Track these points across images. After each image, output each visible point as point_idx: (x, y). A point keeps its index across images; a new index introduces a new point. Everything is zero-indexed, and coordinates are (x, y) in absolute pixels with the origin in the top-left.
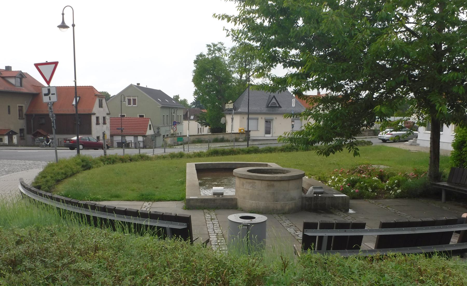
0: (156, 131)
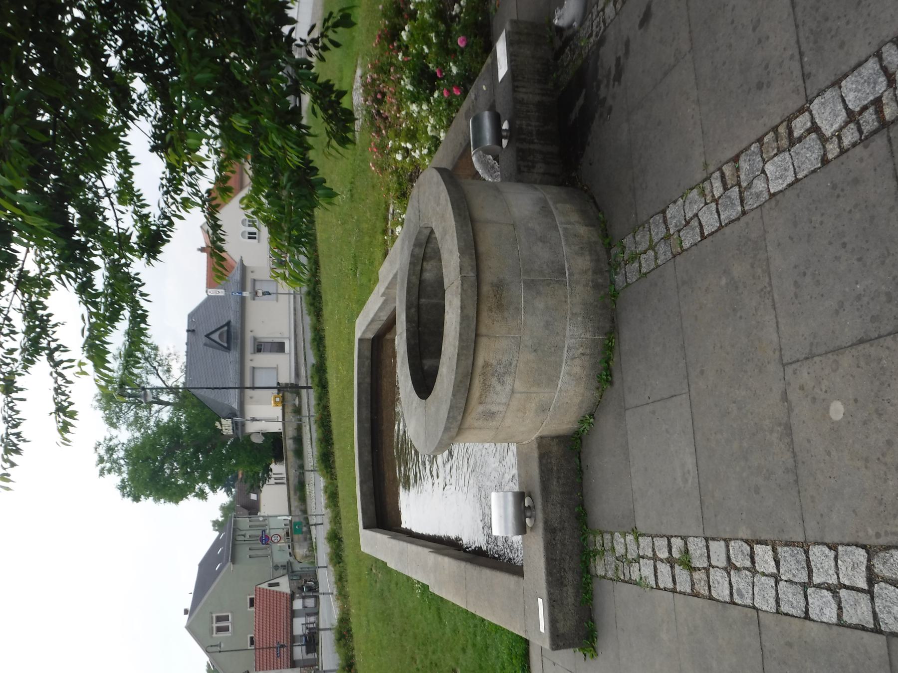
0: (281, 571)
